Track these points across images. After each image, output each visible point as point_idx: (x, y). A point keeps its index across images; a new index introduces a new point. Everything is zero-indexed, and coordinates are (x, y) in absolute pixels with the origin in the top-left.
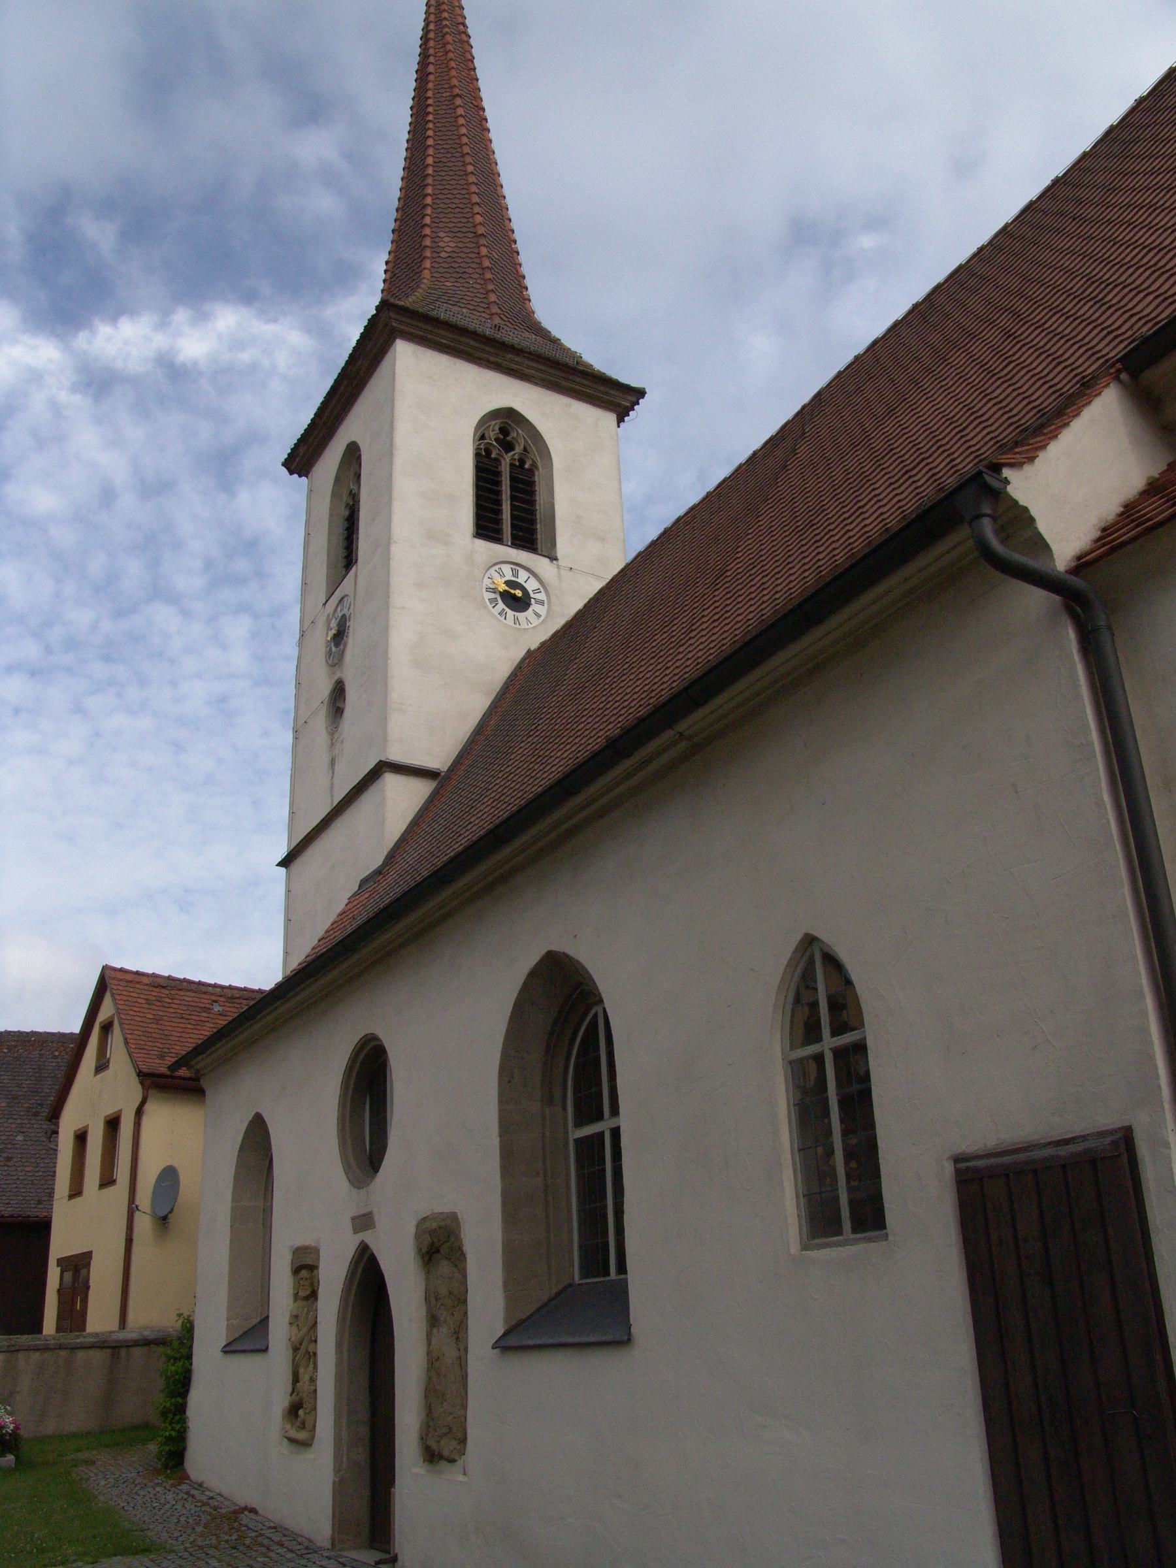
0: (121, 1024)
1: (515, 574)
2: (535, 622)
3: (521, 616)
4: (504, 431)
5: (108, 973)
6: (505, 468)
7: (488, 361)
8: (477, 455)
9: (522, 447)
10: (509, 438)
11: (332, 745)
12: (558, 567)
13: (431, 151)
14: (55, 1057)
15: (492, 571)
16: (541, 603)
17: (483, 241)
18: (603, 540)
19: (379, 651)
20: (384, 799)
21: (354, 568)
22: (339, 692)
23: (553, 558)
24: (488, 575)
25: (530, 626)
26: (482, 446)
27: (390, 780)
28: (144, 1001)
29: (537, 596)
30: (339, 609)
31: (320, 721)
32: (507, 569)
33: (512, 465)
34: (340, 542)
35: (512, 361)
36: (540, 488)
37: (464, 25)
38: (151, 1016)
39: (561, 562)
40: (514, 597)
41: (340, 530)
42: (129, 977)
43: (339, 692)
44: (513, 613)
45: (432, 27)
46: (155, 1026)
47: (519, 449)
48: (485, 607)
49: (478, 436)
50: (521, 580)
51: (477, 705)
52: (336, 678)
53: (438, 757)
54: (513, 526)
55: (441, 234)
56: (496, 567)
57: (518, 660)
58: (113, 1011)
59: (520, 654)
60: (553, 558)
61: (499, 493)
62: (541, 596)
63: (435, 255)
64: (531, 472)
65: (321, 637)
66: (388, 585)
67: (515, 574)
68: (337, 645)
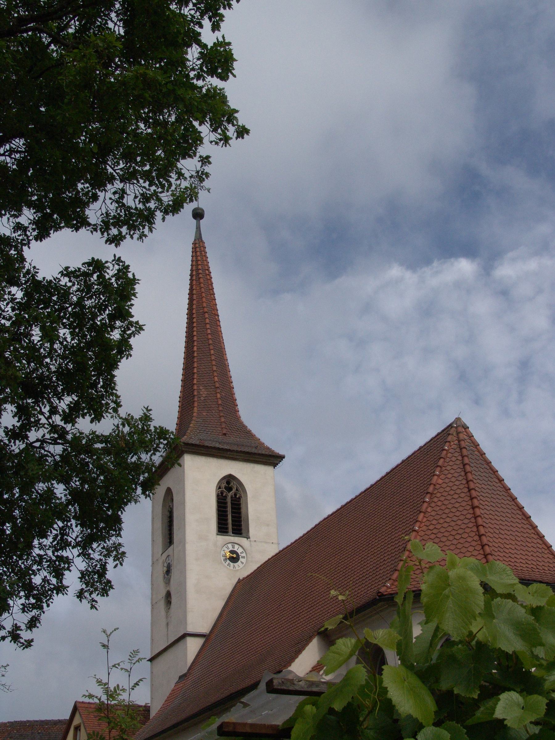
0: (84, 726)
1: (233, 547)
2: (241, 566)
3: (236, 564)
4: (228, 483)
5: (78, 705)
6: (229, 500)
7: (221, 456)
8: (218, 496)
9: (235, 489)
10: (230, 486)
11: (167, 617)
12: (250, 541)
13: (195, 344)
14: (39, 733)
15: (224, 548)
16: (243, 557)
17: (218, 391)
18: (268, 525)
19: (183, 584)
20: (186, 649)
21: (172, 545)
22: (168, 595)
23: (248, 538)
24: (223, 549)
25: (240, 568)
26: (219, 492)
27: (189, 640)
28: (93, 716)
29: (243, 555)
30: (167, 559)
31: (162, 604)
32: (230, 546)
33: (232, 497)
34: (167, 532)
35: (230, 454)
36: (243, 506)
37: (208, 265)
38: (97, 723)
39: (252, 539)
40: (233, 557)
41: (166, 521)
42: (86, 705)
43: (168, 595)
44: (233, 564)
45: (194, 278)
46: (99, 728)
47: (234, 490)
48: (222, 563)
49: (218, 488)
50: (235, 549)
51: (219, 604)
52: (167, 589)
53: (205, 629)
54: (233, 525)
55: (201, 388)
56: (226, 546)
57: (235, 584)
58: (81, 721)
59: (235, 581)
60: (248, 538)
61: (226, 511)
62: (244, 555)
63: (199, 399)
64: (239, 498)
65: (161, 569)
66: (185, 561)
67: (233, 547)
68: (168, 575)
